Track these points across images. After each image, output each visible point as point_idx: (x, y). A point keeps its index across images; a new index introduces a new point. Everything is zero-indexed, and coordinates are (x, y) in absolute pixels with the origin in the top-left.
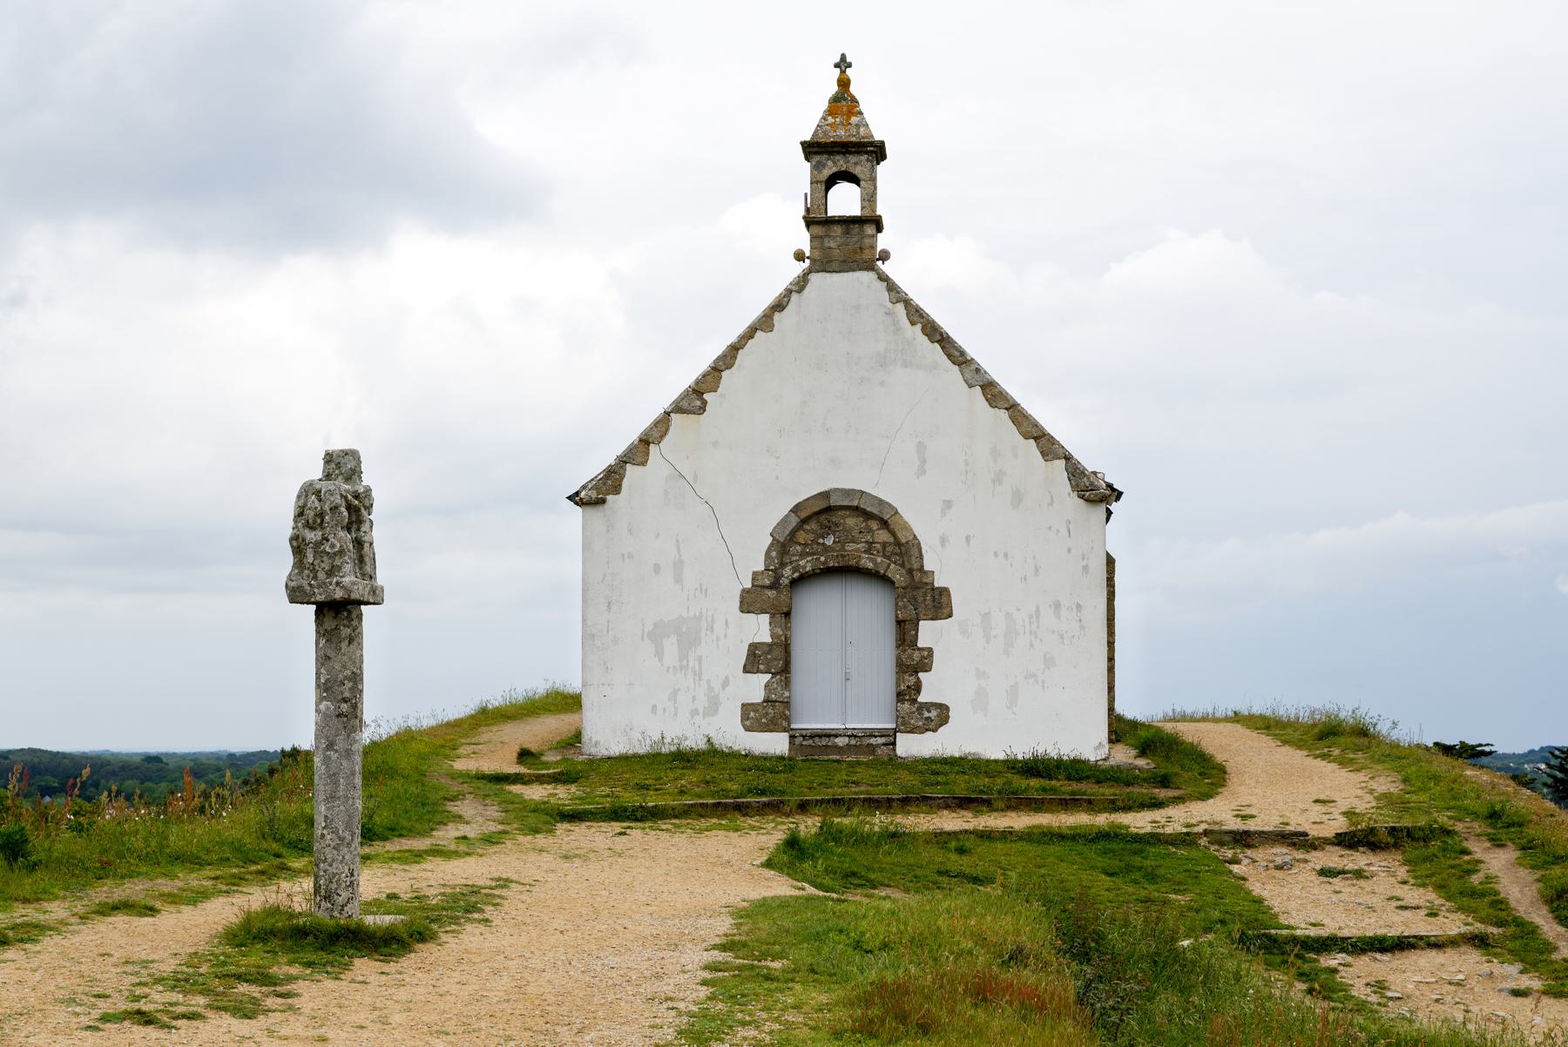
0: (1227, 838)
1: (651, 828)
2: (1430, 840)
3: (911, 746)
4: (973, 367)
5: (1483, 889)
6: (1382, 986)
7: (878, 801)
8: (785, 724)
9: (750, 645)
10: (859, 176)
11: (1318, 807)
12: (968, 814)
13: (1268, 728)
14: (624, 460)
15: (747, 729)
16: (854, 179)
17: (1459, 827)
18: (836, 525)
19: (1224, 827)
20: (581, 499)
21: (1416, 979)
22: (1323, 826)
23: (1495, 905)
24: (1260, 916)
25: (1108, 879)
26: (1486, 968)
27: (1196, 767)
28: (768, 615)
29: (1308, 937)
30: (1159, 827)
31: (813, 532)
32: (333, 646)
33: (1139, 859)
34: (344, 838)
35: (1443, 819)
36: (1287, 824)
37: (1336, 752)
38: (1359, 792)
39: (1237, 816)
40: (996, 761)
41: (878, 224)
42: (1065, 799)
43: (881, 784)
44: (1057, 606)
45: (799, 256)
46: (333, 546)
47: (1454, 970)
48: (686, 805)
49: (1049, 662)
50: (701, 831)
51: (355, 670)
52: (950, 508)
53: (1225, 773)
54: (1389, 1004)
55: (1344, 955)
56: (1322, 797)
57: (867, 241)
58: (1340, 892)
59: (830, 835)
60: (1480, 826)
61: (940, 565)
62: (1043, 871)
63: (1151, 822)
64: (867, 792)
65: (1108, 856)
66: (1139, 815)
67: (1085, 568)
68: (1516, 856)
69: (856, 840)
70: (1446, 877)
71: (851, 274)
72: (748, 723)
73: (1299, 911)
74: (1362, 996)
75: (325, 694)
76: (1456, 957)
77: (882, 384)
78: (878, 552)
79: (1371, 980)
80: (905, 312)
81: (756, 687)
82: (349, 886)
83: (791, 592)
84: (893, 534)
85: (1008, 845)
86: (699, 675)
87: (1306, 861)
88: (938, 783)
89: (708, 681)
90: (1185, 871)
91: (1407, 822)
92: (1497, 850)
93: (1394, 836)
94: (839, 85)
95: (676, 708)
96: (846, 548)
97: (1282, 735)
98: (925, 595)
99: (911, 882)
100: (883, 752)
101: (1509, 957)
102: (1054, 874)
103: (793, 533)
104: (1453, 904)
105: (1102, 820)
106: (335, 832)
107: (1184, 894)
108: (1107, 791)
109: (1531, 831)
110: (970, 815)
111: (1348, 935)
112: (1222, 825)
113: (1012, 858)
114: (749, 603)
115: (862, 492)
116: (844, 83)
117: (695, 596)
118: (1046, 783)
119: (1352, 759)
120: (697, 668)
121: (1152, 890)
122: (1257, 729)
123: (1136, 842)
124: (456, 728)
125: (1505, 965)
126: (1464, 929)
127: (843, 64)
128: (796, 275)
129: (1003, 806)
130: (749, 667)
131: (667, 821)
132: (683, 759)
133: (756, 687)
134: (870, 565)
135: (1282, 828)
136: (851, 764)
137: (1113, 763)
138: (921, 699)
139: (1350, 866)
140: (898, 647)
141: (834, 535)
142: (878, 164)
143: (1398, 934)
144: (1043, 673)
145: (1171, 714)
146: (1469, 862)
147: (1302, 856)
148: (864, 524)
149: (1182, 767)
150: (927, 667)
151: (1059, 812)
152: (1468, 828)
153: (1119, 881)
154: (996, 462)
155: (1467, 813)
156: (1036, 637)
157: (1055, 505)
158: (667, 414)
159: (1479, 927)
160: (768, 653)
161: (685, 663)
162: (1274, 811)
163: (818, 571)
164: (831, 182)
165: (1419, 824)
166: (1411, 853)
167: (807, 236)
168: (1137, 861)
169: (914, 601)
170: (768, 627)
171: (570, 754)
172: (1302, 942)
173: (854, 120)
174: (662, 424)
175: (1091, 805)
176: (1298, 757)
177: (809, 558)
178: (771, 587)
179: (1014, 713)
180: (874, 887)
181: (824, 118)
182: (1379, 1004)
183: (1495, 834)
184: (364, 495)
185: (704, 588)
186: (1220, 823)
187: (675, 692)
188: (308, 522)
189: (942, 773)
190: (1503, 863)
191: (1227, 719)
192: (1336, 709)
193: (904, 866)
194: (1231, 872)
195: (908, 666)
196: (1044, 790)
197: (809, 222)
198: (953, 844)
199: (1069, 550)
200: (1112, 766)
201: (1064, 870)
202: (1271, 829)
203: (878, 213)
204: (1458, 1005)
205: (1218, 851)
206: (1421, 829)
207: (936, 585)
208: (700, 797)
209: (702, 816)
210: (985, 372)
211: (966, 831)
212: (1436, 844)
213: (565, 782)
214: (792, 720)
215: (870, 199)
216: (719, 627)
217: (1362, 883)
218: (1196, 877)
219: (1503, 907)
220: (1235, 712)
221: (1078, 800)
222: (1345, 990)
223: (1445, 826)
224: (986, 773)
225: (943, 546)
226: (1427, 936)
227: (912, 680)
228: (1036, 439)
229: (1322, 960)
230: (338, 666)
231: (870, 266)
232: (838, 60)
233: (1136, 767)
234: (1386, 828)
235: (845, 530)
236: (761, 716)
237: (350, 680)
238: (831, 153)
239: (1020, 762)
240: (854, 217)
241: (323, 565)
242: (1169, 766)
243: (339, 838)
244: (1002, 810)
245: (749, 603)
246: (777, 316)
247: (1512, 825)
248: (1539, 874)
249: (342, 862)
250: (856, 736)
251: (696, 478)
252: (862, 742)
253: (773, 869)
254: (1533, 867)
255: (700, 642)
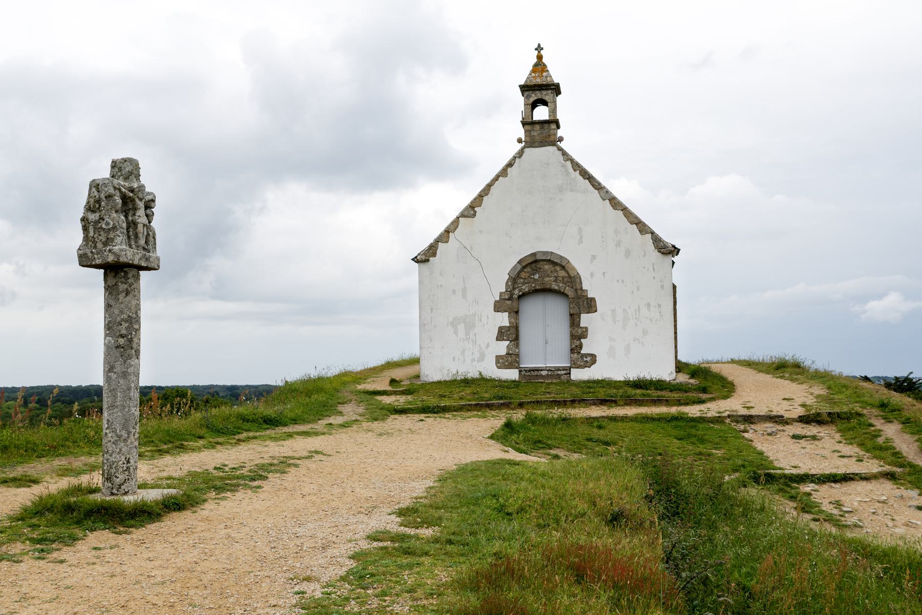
0: (740, 419)
1: (440, 417)
2: (851, 419)
3: (578, 375)
4: (605, 190)
5: (886, 446)
6: (839, 504)
7: (559, 402)
8: (517, 365)
9: (499, 328)
10: (547, 101)
11: (785, 402)
12: (605, 408)
13: (749, 365)
14: (437, 241)
15: (499, 368)
16: (545, 103)
17: (865, 412)
18: (540, 269)
19: (738, 413)
20: (418, 260)
21: (859, 499)
22: (791, 412)
23: (895, 455)
24: (764, 462)
25: (678, 442)
26: (898, 492)
27: (719, 383)
28: (507, 313)
29: (792, 474)
30: (704, 414)
31: (528, 272)
32: (114, 297)
33: (694, 430)
34: (121, 436)
35: (858, 408)
36: (772, 411)
37: (787, 375)
38: (805, 394)
39: (744, 407)
40: (620, 381)
41: (557, 123)
42: (654, 400)
43: (562, 393)
44: (649, 305)
45: (520, 141)
46: (108, 224)
47: (879, 494)
48: (460, 405)
49: (645, 332)
50: (465, 418)
51: (131, 314)
52: (594, 259)
53: (734, 385)
54: (846, 515)
55: (813, 485)
56: (787, 397)
57: (552, 132)
58: (805, 448)
59: (531, 420)
60: (876, 411)
61: (591, 287)
62: (643, 438)
63: (699, 411)
64: (554, 397)
65: (678, 429)
66: (692, 407)
67: (662, 287)
68: (900, 428)
69: (544, 422)
70: (863, 439)
71: (544, 147)
72: (499, 365)
73: (784, 458)
74: (828, 510)
75: (108, 332)
76: (878, 486)
77: (560, 200)
78: (560, 281)
79: (832, 500)
80: (571, 165)
81: (502, 347)
82: (126, 470)
83: (518, 301)
84: (567, 272)
85: (625, 424)
86: (475, 342)
87: (784, 431)
88: (590, 392)
89: (480, 345)
90: (719, 437)
91: (836, 410)
92: (889, 424)
93: (830, 417)
94: (537, 58)
95: (464, 358)
96: (545, 280)
97: (758, 368)
98: (583, 301)
99: (571, 445)
100: (564, 378)
101: (909, 485)
102: (649, 439)
103: (519, 273)
104: (870, 454)
105: (674, 410)
106: (114, 431)
107: (720, 450)
108: (676, 395)
109: (906, 414)
110: (606, 408)
111: (815, 473)
112: (737, 412)
113: (627, 431)
114: (498, 307)
115: (552, 253)
116: (540, 57)
117: (472, 305)
118: (644, 391)
119: (797, 378)
120: (474, 338)
121: (701, 448)
122: (744, 366)
123: (692, 421)
124: (373, 371)
125: (908, 491)
126: (880, 469)
127: (539, 48)
128: (518, 150)
129: (623, 403)
130: (499, 338)
131: (451, 413)
132: (466, 382)
133: (502, 347)
134: (556, 288)
135: (769, 413)
136: (548, 384)
137: (678, 381)
138: (582, 352)
139: (809, 434)
140: (571, 327)
141: (539, 274)
142: (557, 96)
143: (844, 472)
144: (642, 338)
145: (702, 361)
146: (874, 431)
147: (781, 428)
148: (553, 268)
149: (713, 383)
150: (585, 337)
151: (651, 406)
152: (869, 412)
153: (684, 443)
154: (617, 235)
155: (867, 405)
156: (638, 321)
157: (646, 256)
158: (458, 218)
159: (887, 468)
160: (508, 331)
161: (468, 337)
162: (763, 405)
163: (531, 291)
164: (534, 105)
165: (844, 411)
166: (841, 425)
167: (523, 131)
168: (693, 431)
169: (578, 305)
170: (507, 319)
171: (415, 382)
172: (790, 477)
173: (545, 74)
174: (455, 223)
175: (667, 403)
176: (768, 378)
177: (527, 285)
178: (508, 299)
179: (628, 358)
180: (551, 449)
181: (530, 74)
182: (841, 516)
183: (886, 416)
184: (137, 190)
185: (476, 300)
186: (736, 411)
187: (464, 351)
188: (90, 207)
189: (592, 387)
190: (894, 431)
191: (728, 362)
192: (784, 355)
193: (568, 436)
194: (744, 437)
195: (576, 336)
196: (644, 395)
197: (524, 124)
198: (596, 424)
199: (654, 278)
200: (678, 383)
201: (655, 437)
202: (764, 414)
203: (558, 118)
204: (887, 516)
205: (736, 426)
206: (845, 413)
207: (589, 296)
208: (470, 401)
209: (469, 410)
210: (611, 193)
211: (603, 417)
212: (854, 422)
213: (407, 394)
214: (521, 362)
215: (553, 111)
216: (484, 320)
217: (816, 442)
218: (726, 440)
219: (900, 456)
220: (732, 359)
221: (661, 400)
222: (818, 507)
223: (858, 412)
224: (614, 387)
225: (592, 277)
226: (860, 474)
227: (578, 343)
228: (636, 224)
229: (801, 487)
230: (116, 312)
231: (553, 143)
232: (536, 47)
233: (690, 383)
234: (826, 413)
235: (544, 271)
236: (505, 361)
237: (126, 321)
238: (534, 90)
239: (632, 381)
240: (545, 120)
241: (100, 238)
242: (706, 382)
243: (117, 436)
244: (622, 406)
245: (498, 307)
246: (509, 169)
247: (894, 411)
248: (916, 437)
249: (119, 453)
250: (551, 370)
251: (471, 248)
252: (554, 373)
253: (494, 439)
254: (912, 433)
255: (475, 326)
